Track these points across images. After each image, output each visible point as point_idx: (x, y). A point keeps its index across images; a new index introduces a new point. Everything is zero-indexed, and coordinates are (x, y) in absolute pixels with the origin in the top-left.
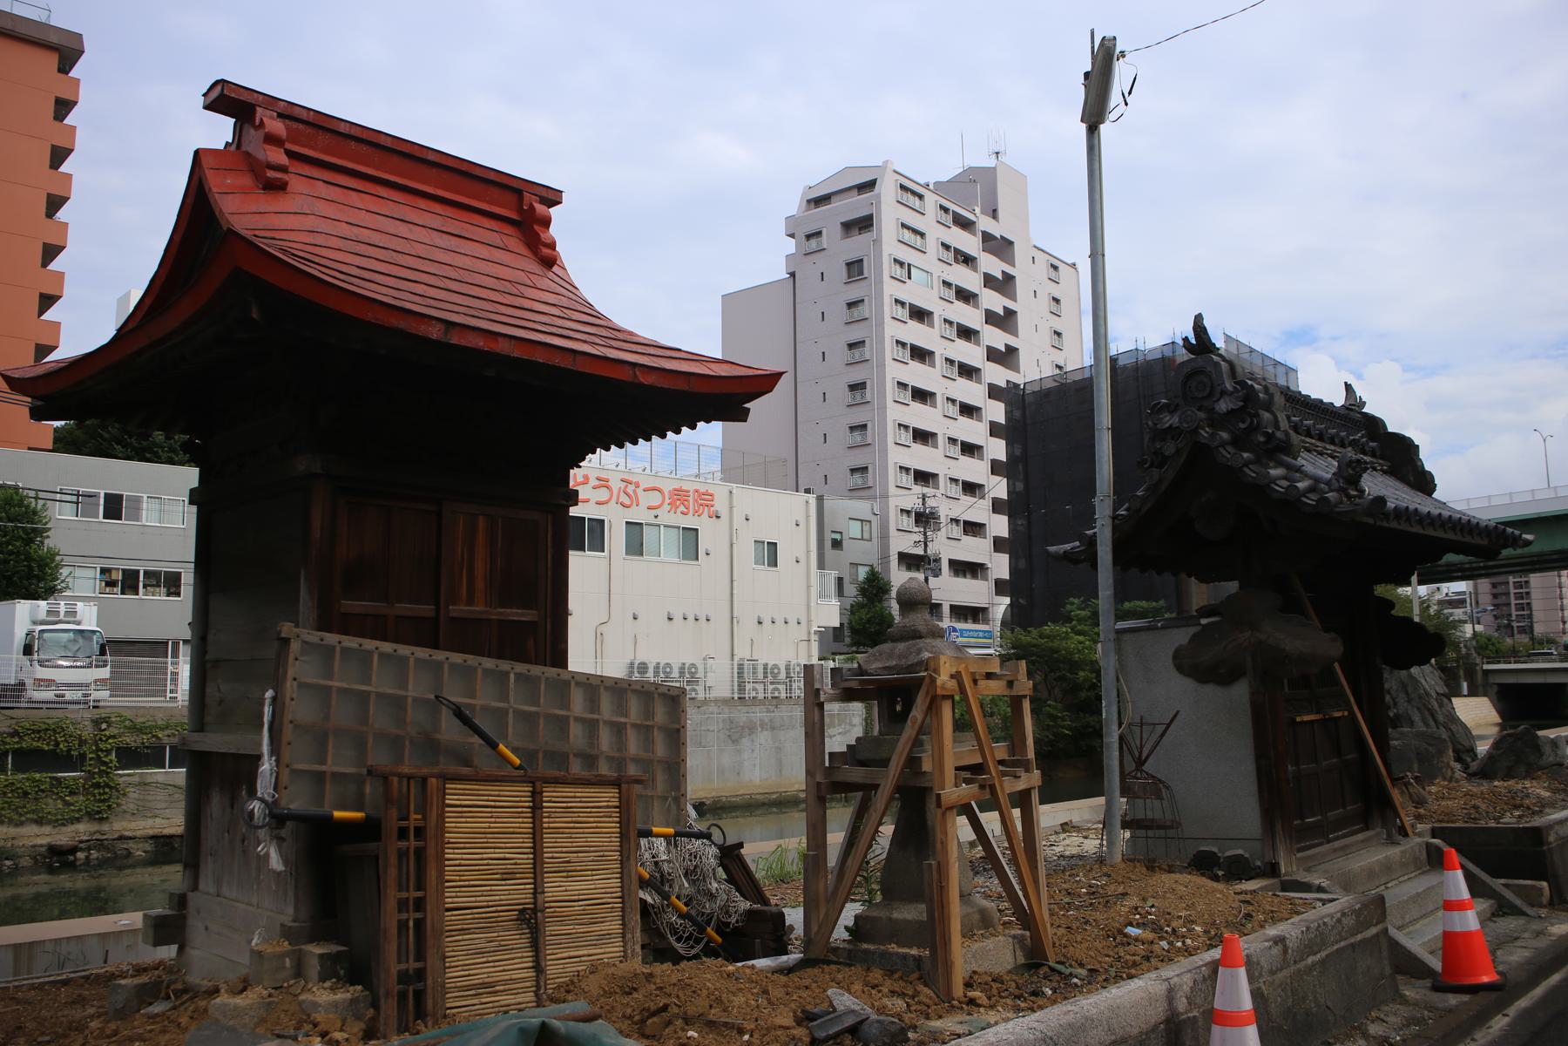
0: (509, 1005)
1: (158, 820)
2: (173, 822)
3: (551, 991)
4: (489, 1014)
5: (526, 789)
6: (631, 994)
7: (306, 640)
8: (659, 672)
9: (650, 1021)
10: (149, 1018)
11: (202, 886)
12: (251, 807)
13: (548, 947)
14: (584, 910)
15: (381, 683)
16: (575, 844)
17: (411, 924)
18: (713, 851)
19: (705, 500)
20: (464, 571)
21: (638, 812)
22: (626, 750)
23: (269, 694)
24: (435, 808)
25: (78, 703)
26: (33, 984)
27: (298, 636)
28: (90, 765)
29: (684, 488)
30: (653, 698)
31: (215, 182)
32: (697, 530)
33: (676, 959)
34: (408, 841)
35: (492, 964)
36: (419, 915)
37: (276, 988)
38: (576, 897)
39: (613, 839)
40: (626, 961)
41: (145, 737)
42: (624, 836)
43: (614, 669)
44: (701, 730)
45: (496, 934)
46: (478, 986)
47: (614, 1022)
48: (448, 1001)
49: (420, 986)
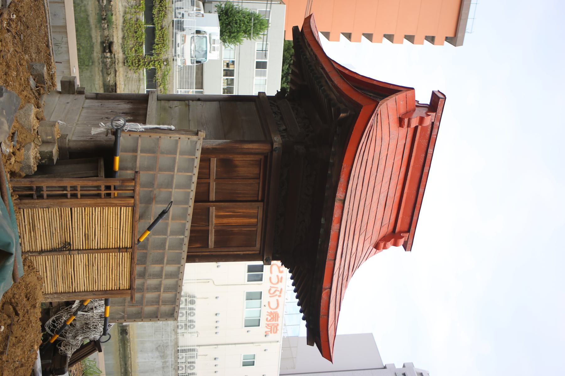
0: (23, 238)
1: (123, 86)
2: (121, 90)
3: (30, 258)
4: (20, 230)
5: (129, 245)
6: (26, 297)
7: (197, 143)
8: (191, 310)
9: (11, 307)
10: (28, 79)
11: (87, 101)
12: (121, 120)
13: (51, 256)
14: (69, 274)
15: (178, 177)
16: (102, 268)
17: (65, 192)
18: (97, 337)
19: (273, 329)
20: (231, 213)
21: (118, 299)
22: (147, 292)
23: (173, 127)
24: (120, 202)
25: (175, 53)
26: (48, 33)
27: (199, 139)
28: (148, 58)
29: (279, 319)
30: (172, 305)
31: (400, 97)
32: (259, 326)
33: (43, 320)
34: (104, 190)
35: (44, 230)
36: (69, 196)
37: (37, 132)
38: (75, 270)
39: (104, 287)
40: (43, 295)
41: (160, 80)
42: (105, 292)
43: (187, 287)
44: (163, 332)
45: (59, 232)
46: (34, 224)
47: (12, 289)
48: (27, 210)
49: (35, 197)
